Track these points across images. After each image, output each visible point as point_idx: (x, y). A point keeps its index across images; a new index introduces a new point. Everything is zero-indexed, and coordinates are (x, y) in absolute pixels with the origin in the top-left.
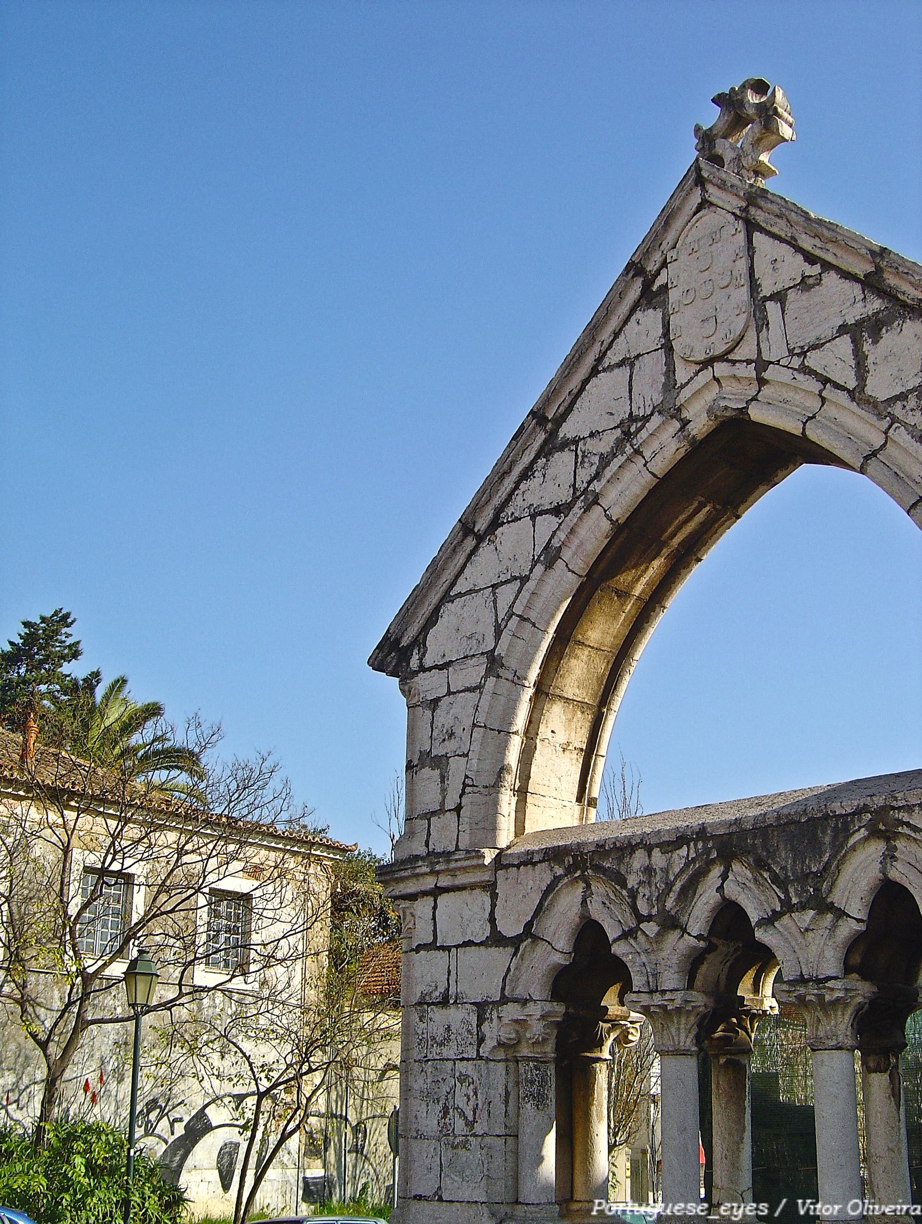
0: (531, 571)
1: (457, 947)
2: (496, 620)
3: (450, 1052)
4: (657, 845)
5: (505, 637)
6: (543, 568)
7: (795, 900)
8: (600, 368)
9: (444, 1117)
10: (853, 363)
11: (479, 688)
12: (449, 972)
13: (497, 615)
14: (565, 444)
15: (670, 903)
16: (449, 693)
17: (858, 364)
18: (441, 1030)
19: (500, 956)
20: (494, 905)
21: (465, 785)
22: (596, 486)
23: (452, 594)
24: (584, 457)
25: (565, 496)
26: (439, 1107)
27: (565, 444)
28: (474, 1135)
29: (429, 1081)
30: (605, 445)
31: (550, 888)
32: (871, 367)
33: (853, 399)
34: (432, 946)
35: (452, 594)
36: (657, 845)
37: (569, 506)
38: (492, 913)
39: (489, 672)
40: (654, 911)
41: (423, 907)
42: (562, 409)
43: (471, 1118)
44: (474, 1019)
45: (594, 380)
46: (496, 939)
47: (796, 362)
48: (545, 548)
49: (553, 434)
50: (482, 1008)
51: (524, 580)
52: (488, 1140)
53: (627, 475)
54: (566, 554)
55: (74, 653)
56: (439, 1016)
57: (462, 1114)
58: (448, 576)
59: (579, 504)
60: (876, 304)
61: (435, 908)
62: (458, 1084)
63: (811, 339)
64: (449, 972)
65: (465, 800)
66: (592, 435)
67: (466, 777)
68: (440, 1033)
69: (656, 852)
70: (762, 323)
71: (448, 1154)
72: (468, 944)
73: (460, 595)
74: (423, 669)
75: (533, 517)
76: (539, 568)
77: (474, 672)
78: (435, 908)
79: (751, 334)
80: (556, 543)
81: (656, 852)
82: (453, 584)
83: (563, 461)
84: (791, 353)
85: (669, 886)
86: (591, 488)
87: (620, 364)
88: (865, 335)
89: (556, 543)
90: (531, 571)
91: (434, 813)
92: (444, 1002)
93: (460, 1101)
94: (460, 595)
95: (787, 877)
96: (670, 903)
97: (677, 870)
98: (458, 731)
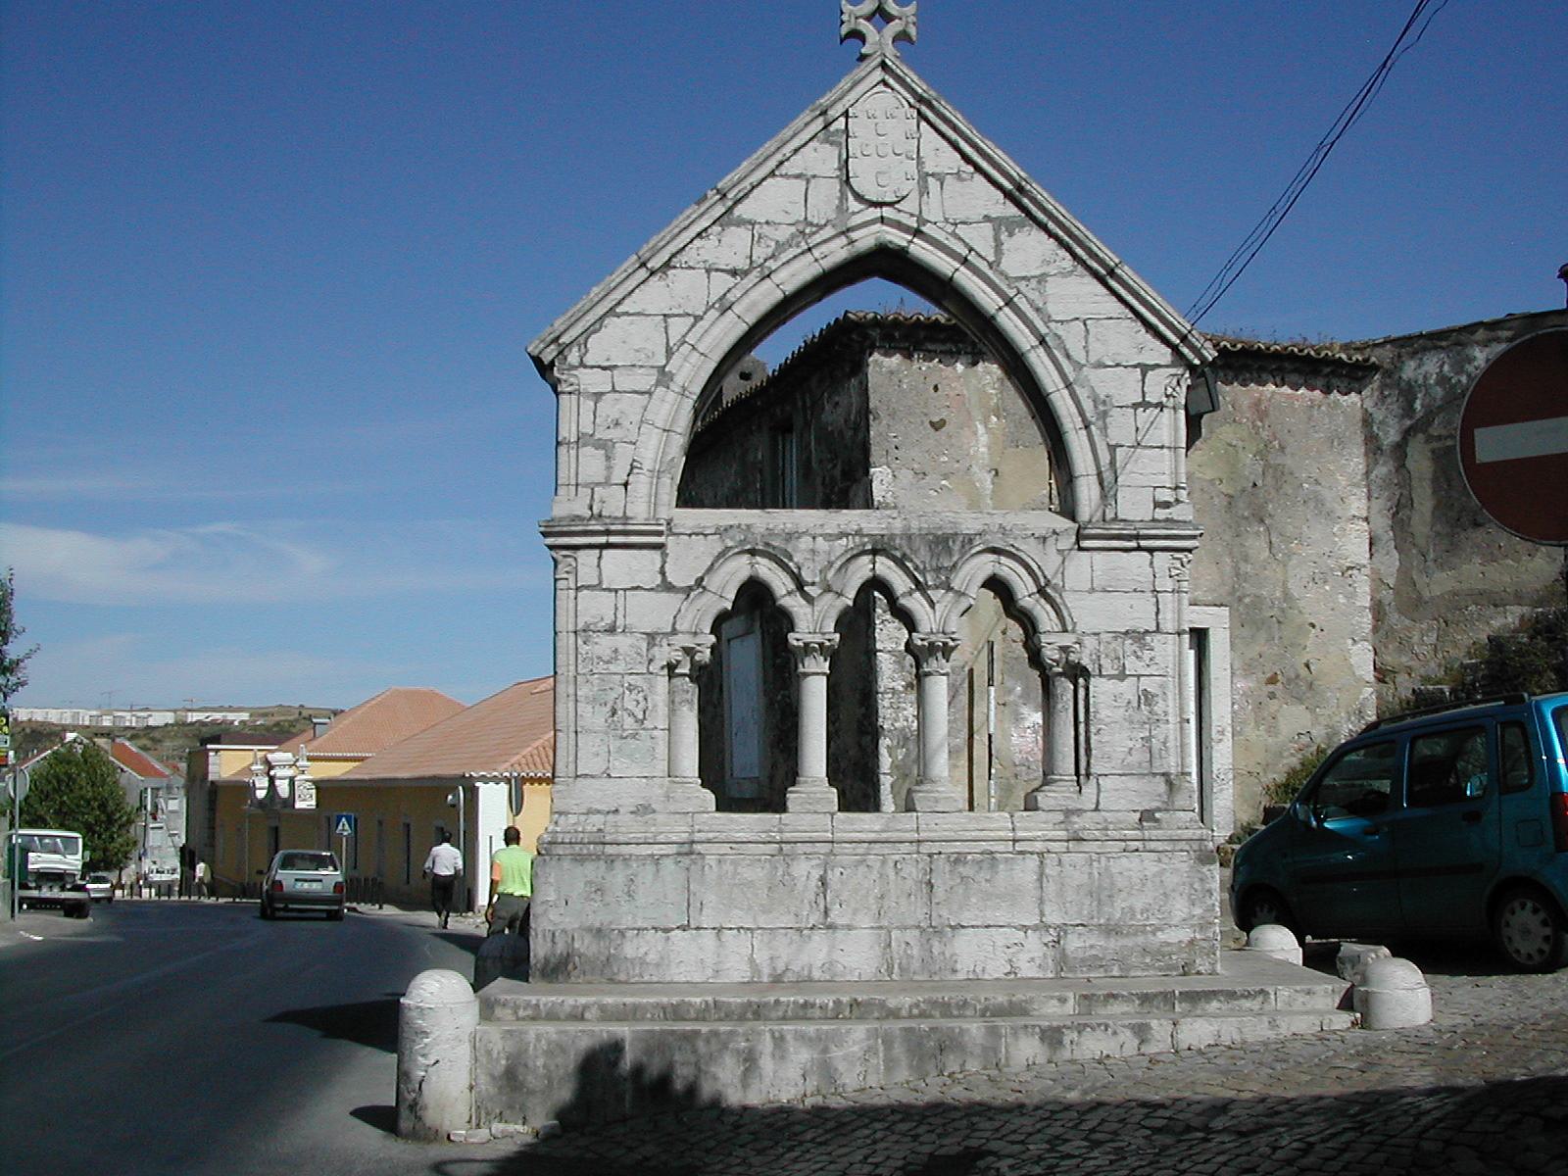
0: (705, 313)
1: (625, 590)
2: (668, 343)
3: (618, 667)
4: (821, 535)
5: (676, 359)
6: (717, 314)
7: (930, 583)
8: (777, 173)
9: (613, 715)
10: (993, 244)
11: (650, 393)
12: (616, 609)
13: (668, 340)
14: (741, 222)
15: (830, 575)
16: (614, 390)
17: (997, 246)
18: (608, 652)
19: (674, 600)
20: (664, 562)
21: (632, 467)
22: (772, 264)
23: (617, 310)
24: (760, 237)
25: (742, 264)
26: (608, 708)
27: (741, 222)
28: (644, 729)
29: (596, 689)
30: (783, 234)
31: (721, 555)
32: (1005, 251)
33: (991, 268)
34: (598, 587)
35: (617, 310)
36: (821, 535)
37: (746, 273)
38: (663, 567)
39: (658, 384)
40: (817, 580)
41: (587, 558)
42: (741, 194)
43: (641, 717)
44: (644, 645)
45: (769, 180)
46: (667, 587)
47: (950, 228)
48: (721, 299)
49: (730, 210)
50: (652, 638)
51: (698, 318)
52: (655, 733)
53: (796, 265)
54: (737, 309)
55: (1011, 235)
56: (604, 644)
57: (632, 714)
58: (617, 295)
59: (755, 273)
60: (1012, 210)
61: (600, 558)
62: (627, 692)
63: (961, 217)
64: (616, 609)
65: (631, 478)
66: (767, 223)
67: (634, 460)
68: (607, 654)
69: (820, 539)
70: (924, 190)
71: (614, 744)
72: (599, 566)
73: (627, 314)
74: (582, 365)
75: (708, 271)
76: (713, 314)
77: (647, 380)
78: (600, 558)
79: (915, 195)
80: (731, 297)
81: (820, 539)
82: (619, 303)
83: (739, 237)
84: (946, 220)
85: (831, 564)
86: (767, 264)
87: (798, 176)
88: (1003, 229)
89: (731, 297)
90: (705, 313)
91: (598, 484)
92: (611, 630)
93: (630, 705)
94: (627, 314)
95: (925, 568)
96: (830, 575)
97: (838, 554)
98: (625, 423)
